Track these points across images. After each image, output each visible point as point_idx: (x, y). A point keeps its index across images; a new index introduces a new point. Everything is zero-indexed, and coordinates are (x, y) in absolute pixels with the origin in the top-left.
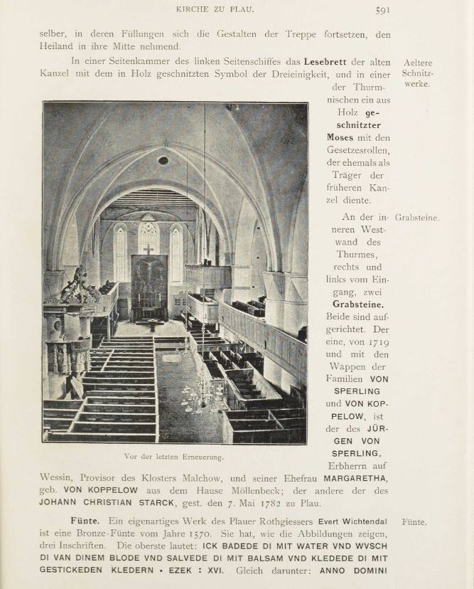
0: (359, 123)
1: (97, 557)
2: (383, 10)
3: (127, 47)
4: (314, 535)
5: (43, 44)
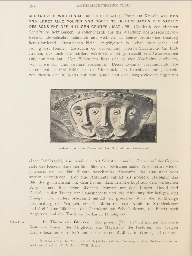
0: (87, 198)
1: (130, 21)
2: (32, 6)
3: (158, 167)
5: (54, 47)
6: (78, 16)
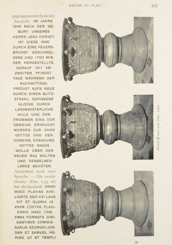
2: (154, 5)
6: (19, 192)
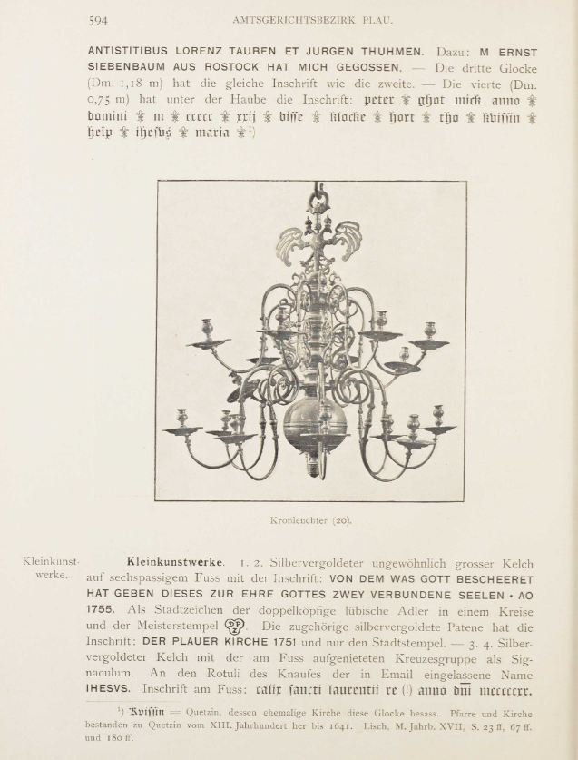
2: (98, 19)
4: (359, 612)
